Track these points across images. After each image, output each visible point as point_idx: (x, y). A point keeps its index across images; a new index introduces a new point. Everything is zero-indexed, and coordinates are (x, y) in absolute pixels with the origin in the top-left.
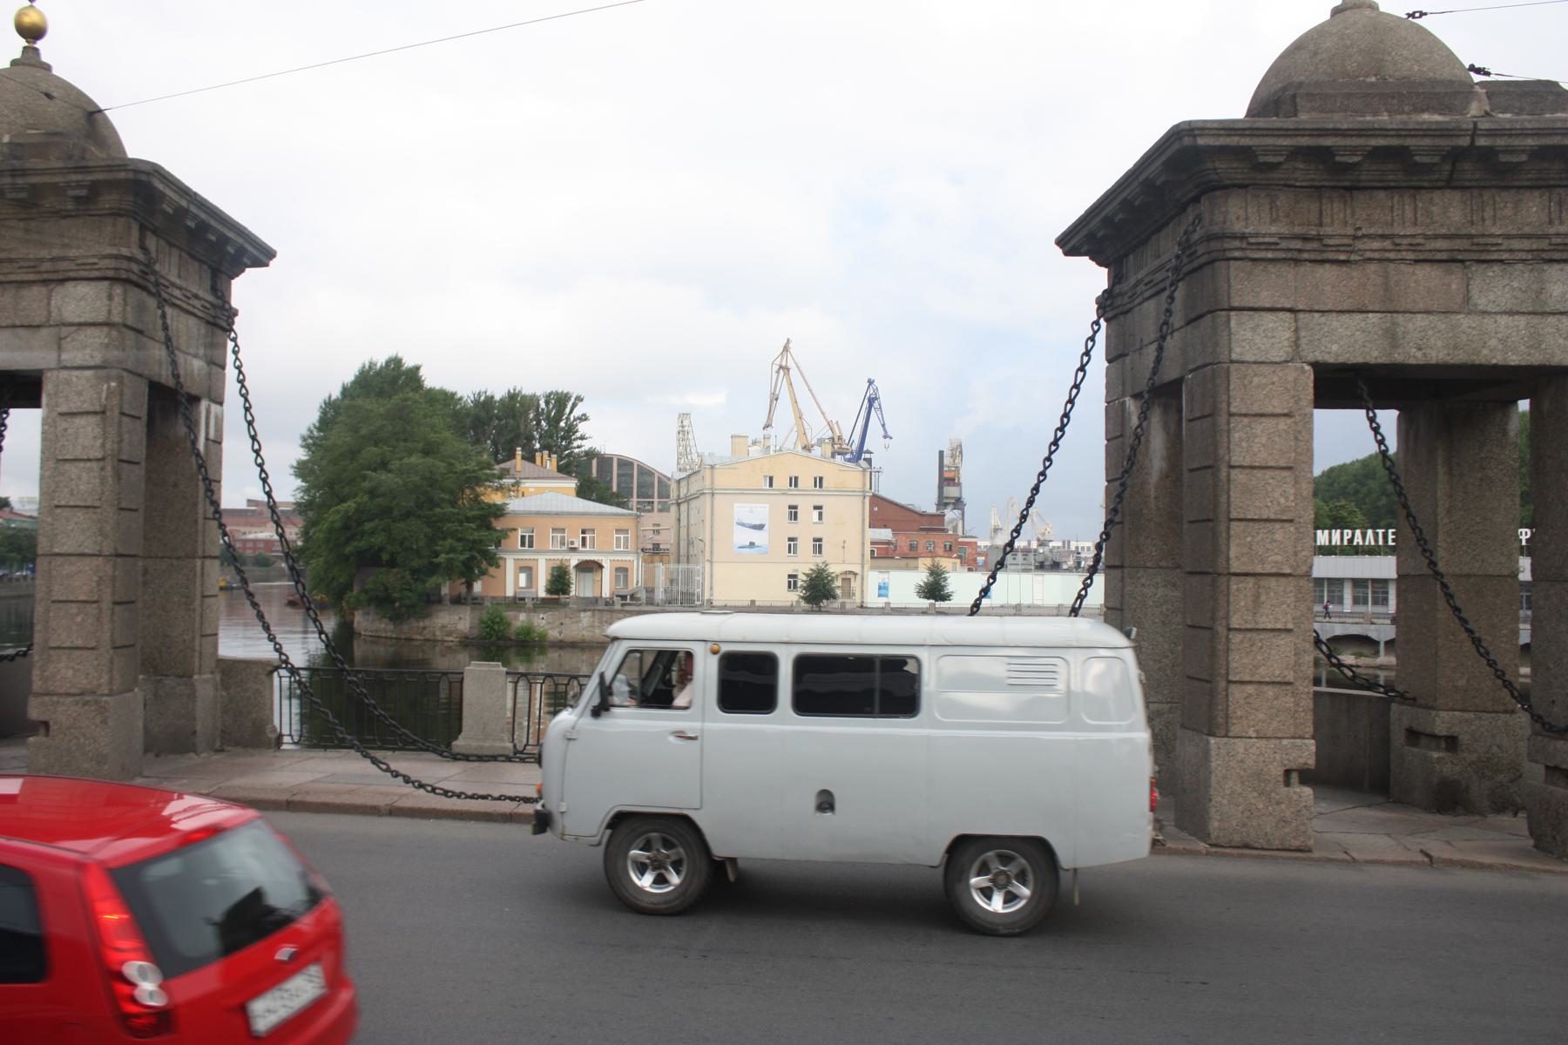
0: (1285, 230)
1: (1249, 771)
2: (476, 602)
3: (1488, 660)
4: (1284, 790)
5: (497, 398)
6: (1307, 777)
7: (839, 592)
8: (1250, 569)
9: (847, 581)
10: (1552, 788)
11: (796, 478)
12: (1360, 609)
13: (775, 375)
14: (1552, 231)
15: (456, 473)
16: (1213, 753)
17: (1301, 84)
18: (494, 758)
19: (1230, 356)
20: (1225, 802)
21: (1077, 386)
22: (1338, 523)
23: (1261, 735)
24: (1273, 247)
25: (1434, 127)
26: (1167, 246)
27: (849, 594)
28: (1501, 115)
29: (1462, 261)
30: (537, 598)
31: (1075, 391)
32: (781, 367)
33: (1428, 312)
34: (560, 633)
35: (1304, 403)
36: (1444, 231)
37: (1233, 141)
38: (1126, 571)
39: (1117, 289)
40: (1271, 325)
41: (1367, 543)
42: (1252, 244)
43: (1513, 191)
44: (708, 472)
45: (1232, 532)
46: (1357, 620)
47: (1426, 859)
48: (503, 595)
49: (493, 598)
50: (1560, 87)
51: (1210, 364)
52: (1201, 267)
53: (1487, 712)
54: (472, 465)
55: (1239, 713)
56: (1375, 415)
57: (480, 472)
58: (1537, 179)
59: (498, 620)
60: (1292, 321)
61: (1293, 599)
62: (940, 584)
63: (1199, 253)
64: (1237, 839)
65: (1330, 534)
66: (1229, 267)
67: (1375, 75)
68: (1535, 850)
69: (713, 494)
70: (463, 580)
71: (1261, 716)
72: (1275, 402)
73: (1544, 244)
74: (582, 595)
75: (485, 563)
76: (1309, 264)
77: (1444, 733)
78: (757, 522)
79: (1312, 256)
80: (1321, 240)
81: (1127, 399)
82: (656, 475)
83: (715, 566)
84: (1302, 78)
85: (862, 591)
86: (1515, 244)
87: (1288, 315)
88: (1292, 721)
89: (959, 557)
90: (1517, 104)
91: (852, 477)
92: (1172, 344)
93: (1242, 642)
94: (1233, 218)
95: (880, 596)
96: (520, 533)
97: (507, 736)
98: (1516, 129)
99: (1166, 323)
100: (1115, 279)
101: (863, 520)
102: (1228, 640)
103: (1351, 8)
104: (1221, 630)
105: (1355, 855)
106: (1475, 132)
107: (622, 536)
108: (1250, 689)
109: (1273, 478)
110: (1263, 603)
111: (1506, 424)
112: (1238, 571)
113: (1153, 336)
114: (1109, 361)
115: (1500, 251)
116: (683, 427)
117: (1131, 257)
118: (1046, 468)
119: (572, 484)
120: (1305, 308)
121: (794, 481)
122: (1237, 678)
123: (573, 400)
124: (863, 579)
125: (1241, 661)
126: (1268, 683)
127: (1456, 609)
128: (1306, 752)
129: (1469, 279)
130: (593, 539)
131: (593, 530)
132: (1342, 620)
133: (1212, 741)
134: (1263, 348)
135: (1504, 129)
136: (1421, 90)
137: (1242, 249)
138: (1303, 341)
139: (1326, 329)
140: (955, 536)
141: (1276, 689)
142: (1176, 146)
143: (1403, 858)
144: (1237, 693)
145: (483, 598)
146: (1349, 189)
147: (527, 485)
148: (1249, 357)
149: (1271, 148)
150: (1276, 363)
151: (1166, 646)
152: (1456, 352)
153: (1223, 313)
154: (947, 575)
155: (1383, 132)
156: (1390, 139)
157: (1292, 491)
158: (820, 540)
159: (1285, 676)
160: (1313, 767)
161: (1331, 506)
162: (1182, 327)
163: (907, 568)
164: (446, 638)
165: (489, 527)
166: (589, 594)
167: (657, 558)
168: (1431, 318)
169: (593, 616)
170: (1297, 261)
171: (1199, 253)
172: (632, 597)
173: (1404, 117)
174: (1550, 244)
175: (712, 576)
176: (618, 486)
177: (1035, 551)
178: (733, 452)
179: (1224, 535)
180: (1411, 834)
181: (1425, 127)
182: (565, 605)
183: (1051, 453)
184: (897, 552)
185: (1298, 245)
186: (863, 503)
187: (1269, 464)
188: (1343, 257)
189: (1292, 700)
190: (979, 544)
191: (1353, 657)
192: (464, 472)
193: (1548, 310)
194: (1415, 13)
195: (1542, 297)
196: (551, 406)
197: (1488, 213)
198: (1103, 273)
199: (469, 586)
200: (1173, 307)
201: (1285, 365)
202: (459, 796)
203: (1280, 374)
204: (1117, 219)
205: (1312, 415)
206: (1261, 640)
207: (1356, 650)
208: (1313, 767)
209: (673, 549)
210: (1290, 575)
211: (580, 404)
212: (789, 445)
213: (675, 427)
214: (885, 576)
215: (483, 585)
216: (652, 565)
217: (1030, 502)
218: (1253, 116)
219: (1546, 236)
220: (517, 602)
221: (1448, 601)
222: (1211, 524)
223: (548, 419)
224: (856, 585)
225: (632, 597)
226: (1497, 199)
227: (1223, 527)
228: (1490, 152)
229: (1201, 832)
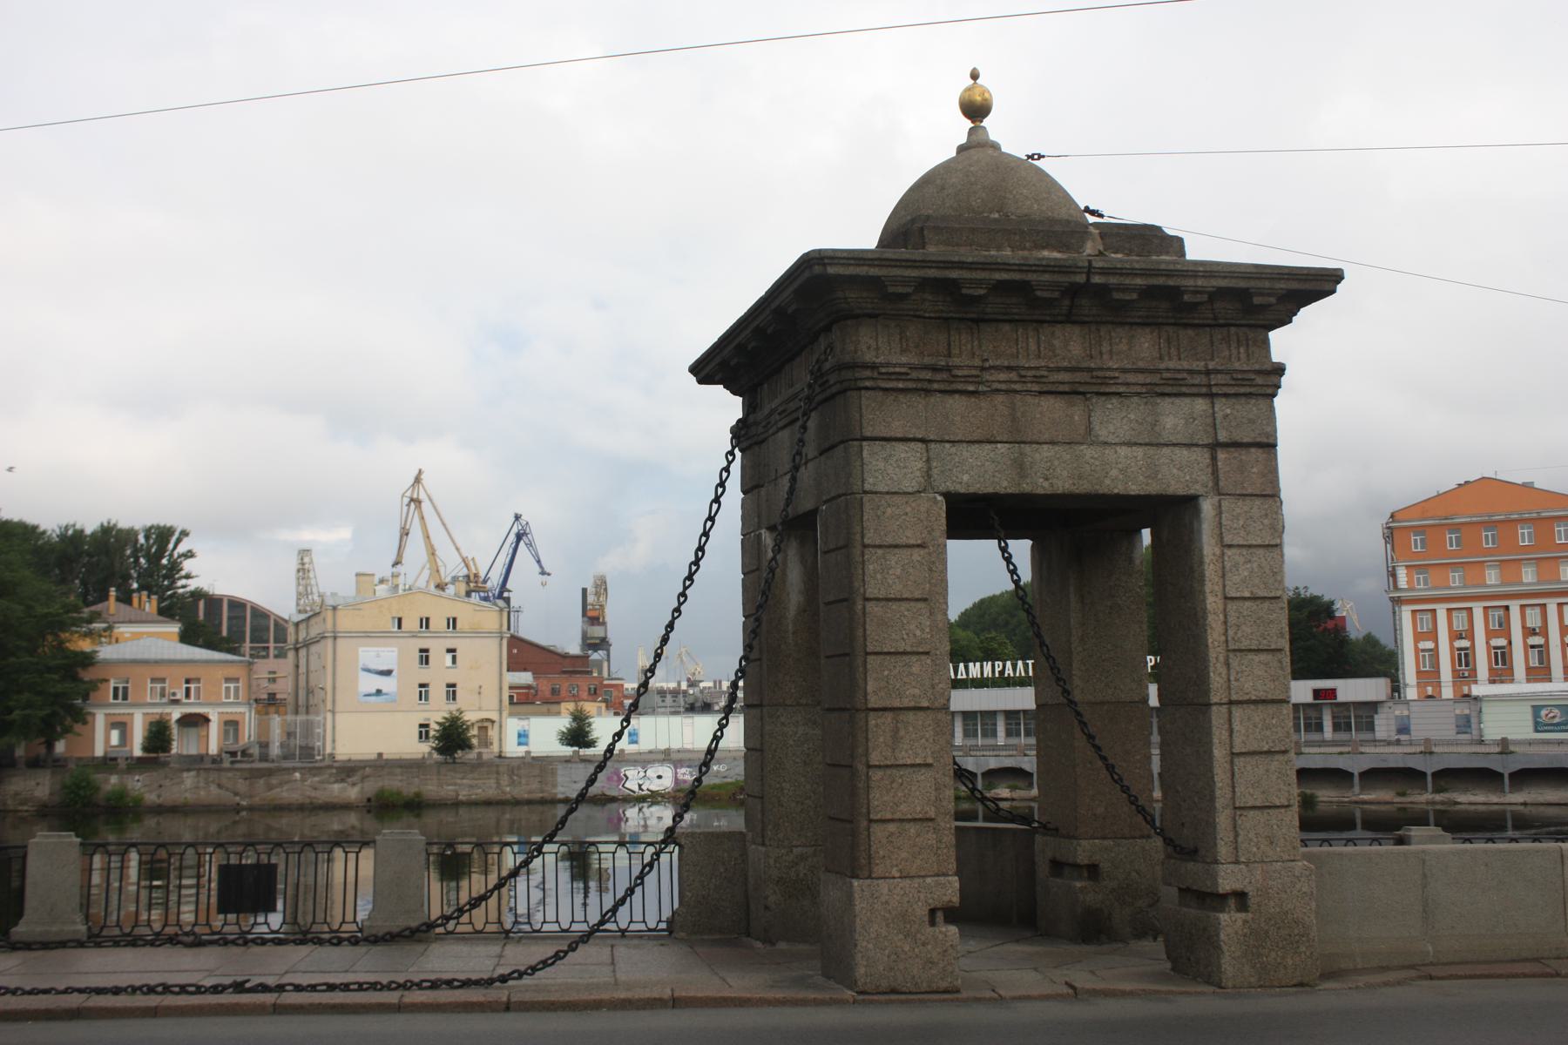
0: (915, 361)
1: (894, 913)
2: (58, 764)
3: (1122, 786)
4: (930, 930)
5: (88, 531)
6: (952, 915)
7: (475, 741)
8: (888, 704)
9: (483, 729)
10: (1185, 909)
11: (427, 619)
12: (1013, 741)
13: (405, 508)
14: (1162, 366)
15: (35, 617)
16: (856, 895)
17: (928, 217)
18: (63, 944)
19: (863, 486)
20: (871, 946)
21: (711, 518)
22: (989, 655)
23: (904, 874)
24: (904, 377)
25: (1052, 264)
26: (799, 376)
27: (486, 743)
28: (1113, 255)
29: (1083, 394)
30: (132, 758)
31: (709, 524)
32: (412, 500)
33: (1053, 443)
34: (159, 796)
35: (937, 534)
36: (1065, 364)
37: (863, 271)
38: (765, 710)
39: (751, 419)
40: (903, 455)
41: (1018, 675)
42: (882, 374)
43: (1127, 328)
44: (329, 614)
45: (869, 666)
46: (1011, 753)
47: (1071, 991)
48: (89, 755)
49: (80, 759)
50: (1163, 232)
51: (844, 495)
52: (833, 396)
53: (1125, 838)
54: (55, 608)
55: (881, 853)
56: (1006, 544)
57: (65, 616)
58: (1147, 317)
59: (84, 784)
60: (924, 451)
61: (932, 733)
62: (584, 730)
63: (832, 382)
64: (884, 984)
65: (982, 667)
66: (860, 397)
67: (998, 212)
68: (1172, 973)
69: (335, 638)
70: (43, 740)
71: (904, 855)
72: (909, 533)
73: (1156, 379)
74: (185, 753)
75: (69, 719)
76: (939, 395)
77: (1086, 862)
78: (385, 668)
79: (942, 386)
80: (950, 371)
81: (763, 531)
82: (272, 618)
83: (339, 717)
84: (931, 212)
85: (500, 740)
86: (1131, 378)
87: (920, 445)
88: (934, 859)
89: (605, 701)
90: (1127, 246)
91: (489, 618)
92: (806, 475)
93: (882, 779)
94: (864, 349)
95: (519, 744)
96: (112, 684)
97: (79, 917)
98: (1126, 269)
99: (799, 453)
100: (749, 408)
101: (501, 663)
102: (868, 777)
103: (974, 147)
104: (861, 768)
105: (1002, 993)
106: (1090, 270)
108: (892, 827)
109: (908, 610)
110: (902, 738)
111: (1132, 552)
112: (876, 706)
113: (788, 467)
114: (744, 492)
115: (1117, 384)
116: (303, 564)
117: (766, 385)
118: (680, 604)
119: (174, 628)
120: (936, 438)
121: (425, 623)
122: (879, 817)
123: (176, 535)
124: (501, 726)
125: (882, 798)
126: (909, 821)
127: (1090, 737)
128: (950, 890)
129: (1090, 410)
130: (198, 690)
131: (198, 680)
132: (995, 753)
133: (856, 883)
134: (895, 478)
135: (1116, 268)
136: (1040, 228)
137: (873, 379)
138: (935, 472)
139: (957, 460)
140: (601, 678)
141: (918, 826)
142: (807, 274)
143: (1049, 992)
144: (878, 832)
145: (66, 760)
146: (977, 321)
147: (121, 630)
148: (882, 488)
149: (899, 279)
150: (909, 493)
151: (808, 787)
152: (1081, 482)
153: (855, 443)
154: (591, 720)
155: (1005, 266)
156: (1012, 273)
157: (928, 623)
158: (454, 685)
159: (926, 813)
160: (958, 905)
161: (983, 638)
162: (816, 458)
163: (549, 714)
164: (20, 808)
165: (75, 678)
166: (193, 751)
167: (272, 709)
168: (1057, 448)
169: (198, 776)
170: (928, 392)
171: (832, 382)
172: (244, 753)
173: (1026, 253)
174: (1162, 379)
175: (334, 727)
176: (229, 629)
177: (685, 692)
178: (358, 591)
179: (861, 669)
180: (1055, 967)
181: (1044, 263)
182: (165, 764)
183: (685, 588)
184: (538, 697)
185: (928, 375)
186: (501, 645)
187: (905, 596)
188: (971, 388)
189: (934, 836)
190: (626, 686)
191: (1007, 790)
192: (46, 615)
193: (1162, 441)
194: (1033, 155)
195: (1157, 428)
196: (151, 541)
197: (1105, 347)
198: (738, 401)
199: (50, 746)
200: (806, 437)
201: (918, 495)
202: (14, 992)
203: (913, 505)
204: (750, 347)
205: (945, 546)
206: (901, 777)
207: (1011, 783)
208: (958, 905)
209: (290, 699)
210: (928, 708)
211: (185, 540)
212: (422, 583)
213: (293, 564)
214: (525, 723)
215: (67, 747)
216: (265, 717)
217: (665, 640)
218: (883, 247)
219: (1157, 371)
220: (108, 763)
221: (1083, 731)
222: (847, 658)
223: (148, 556)
224: (493, 733)
225: (244, 753)
226: (1113, 334)
227: (859, 661)
228: (1104, 290)
229: (851, 984)
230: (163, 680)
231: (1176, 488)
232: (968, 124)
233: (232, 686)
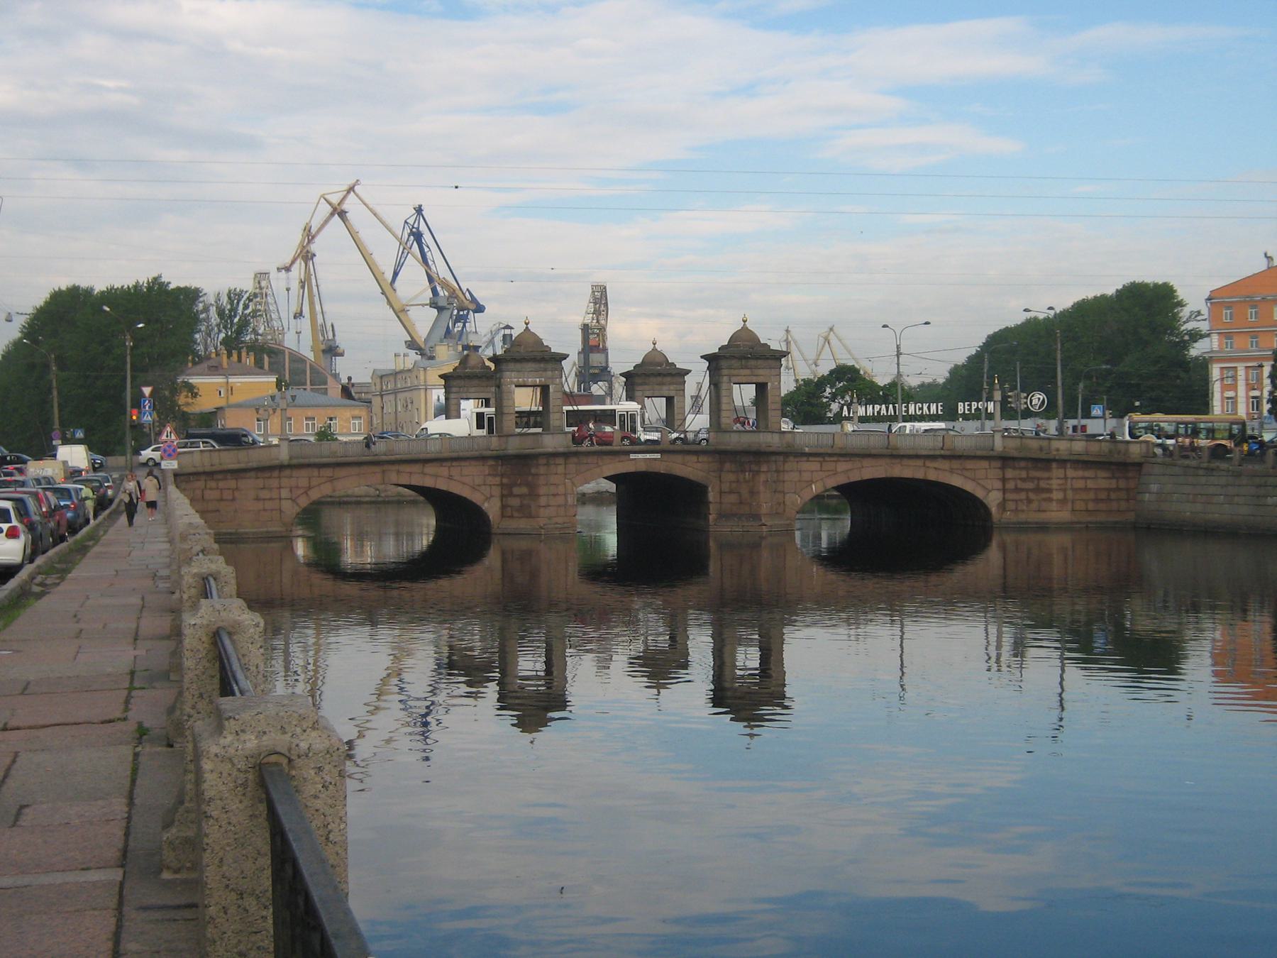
41: (889, 414)
82: (287, 351)
107: (310, 422)
116: (261, 288)
231: (672, 395)
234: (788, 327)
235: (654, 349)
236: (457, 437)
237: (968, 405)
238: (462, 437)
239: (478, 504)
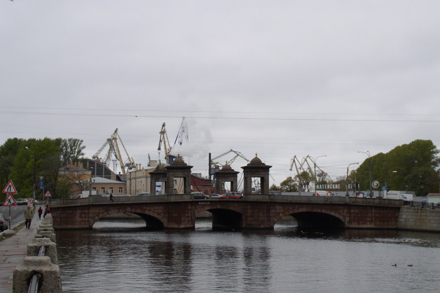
41: (320, 188)
230: (104, 188)
232: (256, 156)
233: (121, 189)
234: (296, 155)
235: (256, 157)
236: (322, 196)
237: (326, 186)
238: (305, 196)
239: (160, 220)
